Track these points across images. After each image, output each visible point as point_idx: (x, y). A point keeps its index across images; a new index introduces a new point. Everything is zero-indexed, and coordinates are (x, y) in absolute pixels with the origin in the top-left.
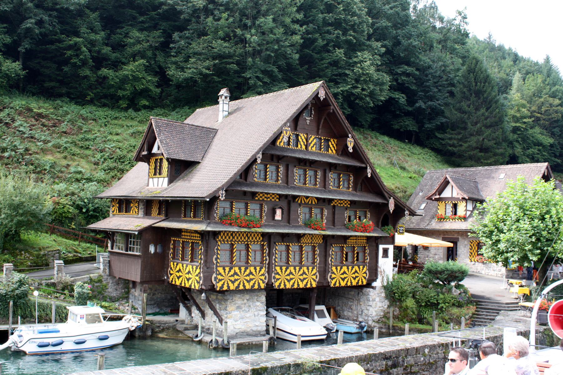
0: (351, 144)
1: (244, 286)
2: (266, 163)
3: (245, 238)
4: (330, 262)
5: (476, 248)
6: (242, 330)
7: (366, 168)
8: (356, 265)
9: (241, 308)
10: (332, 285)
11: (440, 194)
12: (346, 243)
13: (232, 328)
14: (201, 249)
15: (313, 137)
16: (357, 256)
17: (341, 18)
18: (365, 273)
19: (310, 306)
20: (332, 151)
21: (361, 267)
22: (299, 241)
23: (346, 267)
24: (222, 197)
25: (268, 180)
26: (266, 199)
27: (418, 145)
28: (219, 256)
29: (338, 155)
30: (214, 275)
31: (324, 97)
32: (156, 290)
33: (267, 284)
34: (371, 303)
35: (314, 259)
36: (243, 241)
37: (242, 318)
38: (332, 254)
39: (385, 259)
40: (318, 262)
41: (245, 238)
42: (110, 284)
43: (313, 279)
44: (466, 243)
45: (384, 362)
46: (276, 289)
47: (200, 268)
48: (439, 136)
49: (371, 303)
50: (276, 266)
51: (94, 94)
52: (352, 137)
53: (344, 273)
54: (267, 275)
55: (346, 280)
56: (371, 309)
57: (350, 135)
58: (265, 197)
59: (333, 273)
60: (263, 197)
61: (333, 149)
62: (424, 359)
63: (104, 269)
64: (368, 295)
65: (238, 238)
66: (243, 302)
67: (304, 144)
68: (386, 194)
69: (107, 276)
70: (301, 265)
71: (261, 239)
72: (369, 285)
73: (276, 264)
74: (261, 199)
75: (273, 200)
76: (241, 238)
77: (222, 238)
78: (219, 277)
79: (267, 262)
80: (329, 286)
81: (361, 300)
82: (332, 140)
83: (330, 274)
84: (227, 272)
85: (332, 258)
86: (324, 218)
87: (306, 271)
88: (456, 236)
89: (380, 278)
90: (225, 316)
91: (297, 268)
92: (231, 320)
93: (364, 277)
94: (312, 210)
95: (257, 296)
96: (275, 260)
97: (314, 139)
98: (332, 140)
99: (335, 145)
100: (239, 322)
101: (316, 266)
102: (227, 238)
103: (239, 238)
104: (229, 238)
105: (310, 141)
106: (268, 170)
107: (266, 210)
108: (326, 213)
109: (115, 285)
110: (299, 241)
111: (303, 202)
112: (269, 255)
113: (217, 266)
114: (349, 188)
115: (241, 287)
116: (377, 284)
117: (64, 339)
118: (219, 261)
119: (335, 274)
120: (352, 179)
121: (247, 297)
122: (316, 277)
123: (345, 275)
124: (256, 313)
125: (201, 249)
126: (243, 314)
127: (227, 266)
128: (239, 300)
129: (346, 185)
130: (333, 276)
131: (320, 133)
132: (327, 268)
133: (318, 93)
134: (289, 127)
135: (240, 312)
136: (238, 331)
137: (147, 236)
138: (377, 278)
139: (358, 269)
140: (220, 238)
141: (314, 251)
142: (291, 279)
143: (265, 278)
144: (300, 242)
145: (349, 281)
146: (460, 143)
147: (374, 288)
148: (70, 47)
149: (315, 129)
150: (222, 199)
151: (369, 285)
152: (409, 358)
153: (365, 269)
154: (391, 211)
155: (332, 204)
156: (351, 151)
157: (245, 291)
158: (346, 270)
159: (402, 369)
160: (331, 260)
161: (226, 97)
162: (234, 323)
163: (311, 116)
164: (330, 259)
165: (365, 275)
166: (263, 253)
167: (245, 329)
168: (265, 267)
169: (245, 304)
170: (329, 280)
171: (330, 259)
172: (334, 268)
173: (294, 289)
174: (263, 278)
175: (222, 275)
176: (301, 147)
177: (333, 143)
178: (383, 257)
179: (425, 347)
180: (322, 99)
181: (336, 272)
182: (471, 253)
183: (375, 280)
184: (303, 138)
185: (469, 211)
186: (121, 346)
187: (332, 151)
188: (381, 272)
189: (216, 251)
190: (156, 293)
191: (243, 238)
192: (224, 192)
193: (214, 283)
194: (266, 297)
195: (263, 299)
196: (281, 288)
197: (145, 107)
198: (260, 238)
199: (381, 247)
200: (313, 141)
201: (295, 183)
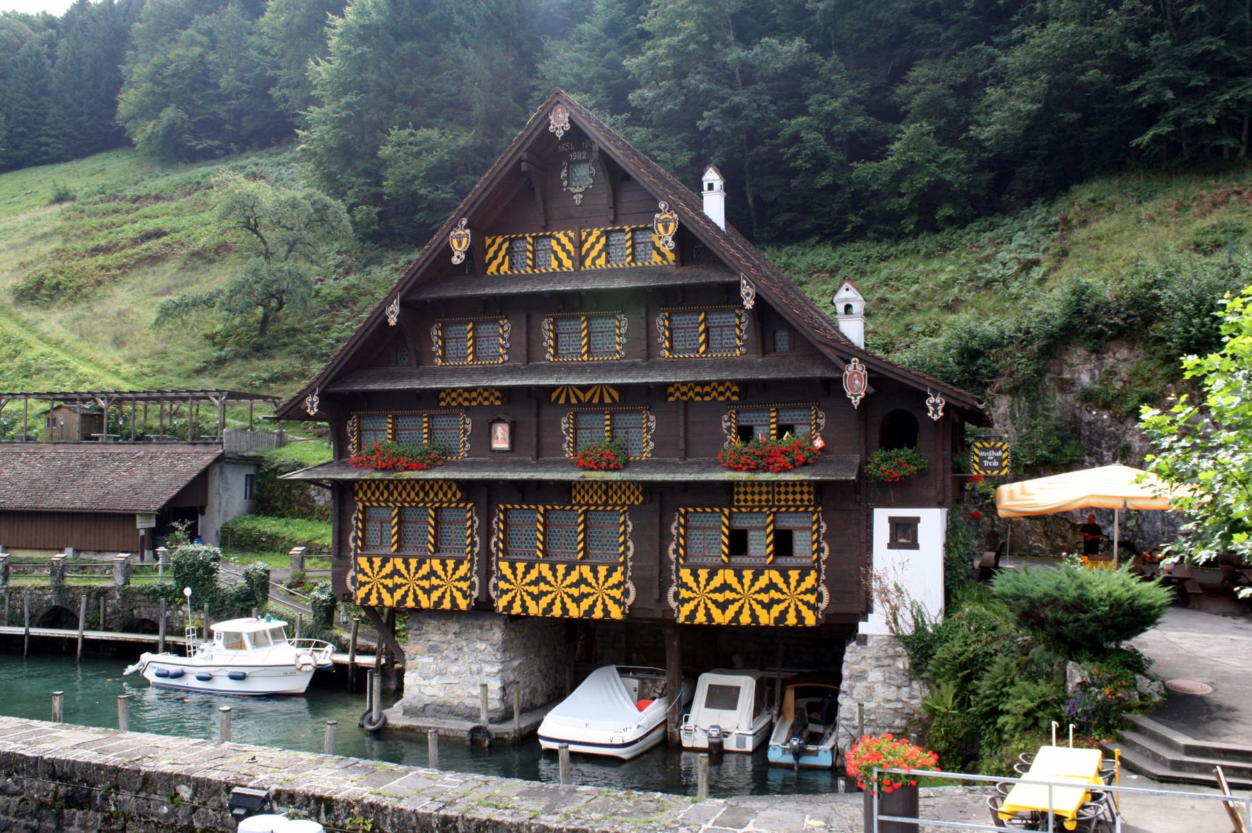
1: (416, 599)
3: (417, 494)
6: (440, 701)
9: (440, 652)
10: (681, 619)
13: (415, 691)
15: (596, 233)
26: (466, 404)
30: (352, 573)
36: (413, 500)
38: (499, 529)
41: (417, 494)
45: (53, 785)
50: (498, 559)
51: (863, 216)
54: (475, 579)
58: (466, 399)
62: (172, 813)
65: (400, 494)
66: (443, 638)
67: (569, 257)
71: (459, 495)
74: (454, 404)
75: (486, 403)
76: (409, 495)
77: (365, 493)
78: (361, 577)
84: (560, 577)
85: (678, 545)
92: (415, 675)
95: (420, 622)
100: (433, 682)
102: (377, 494)
103: (404, 495)
104: (382, 494)
111: (574, 401)
113: (356, 555)
115: (410, 603)
116: (874, 626)
117: (186, 669)
121: (455, 627)
124: (475, 667)
126: (442, 665)
128: (435, 634)
134: (466, 227)
135: (435, 659)
136: (428, 700)
138: (869, 609)
140: (361, 494)
142: (543, 594)
143: (472, 587)
147: (863, 640)
150: (312, 413)
152: (126, 796)
159: (99, 816)
160: (496, 544)
162: (421, 682)
167: (446, 699)
168: (471, 561)
169: (449, 643)
175: (366, 574)
176: (561, 265)
178: (891, 546)
179: (187, 780)
184: (564, 240)
186: (304, 701)
188: (885, 592)
191: (413, 495)
192: (315, 399)
193: (352, 588)
196: (696, 622)
197: (950, 220)
198: (454, 495)
199: (882, 518)
201: (547, 356)
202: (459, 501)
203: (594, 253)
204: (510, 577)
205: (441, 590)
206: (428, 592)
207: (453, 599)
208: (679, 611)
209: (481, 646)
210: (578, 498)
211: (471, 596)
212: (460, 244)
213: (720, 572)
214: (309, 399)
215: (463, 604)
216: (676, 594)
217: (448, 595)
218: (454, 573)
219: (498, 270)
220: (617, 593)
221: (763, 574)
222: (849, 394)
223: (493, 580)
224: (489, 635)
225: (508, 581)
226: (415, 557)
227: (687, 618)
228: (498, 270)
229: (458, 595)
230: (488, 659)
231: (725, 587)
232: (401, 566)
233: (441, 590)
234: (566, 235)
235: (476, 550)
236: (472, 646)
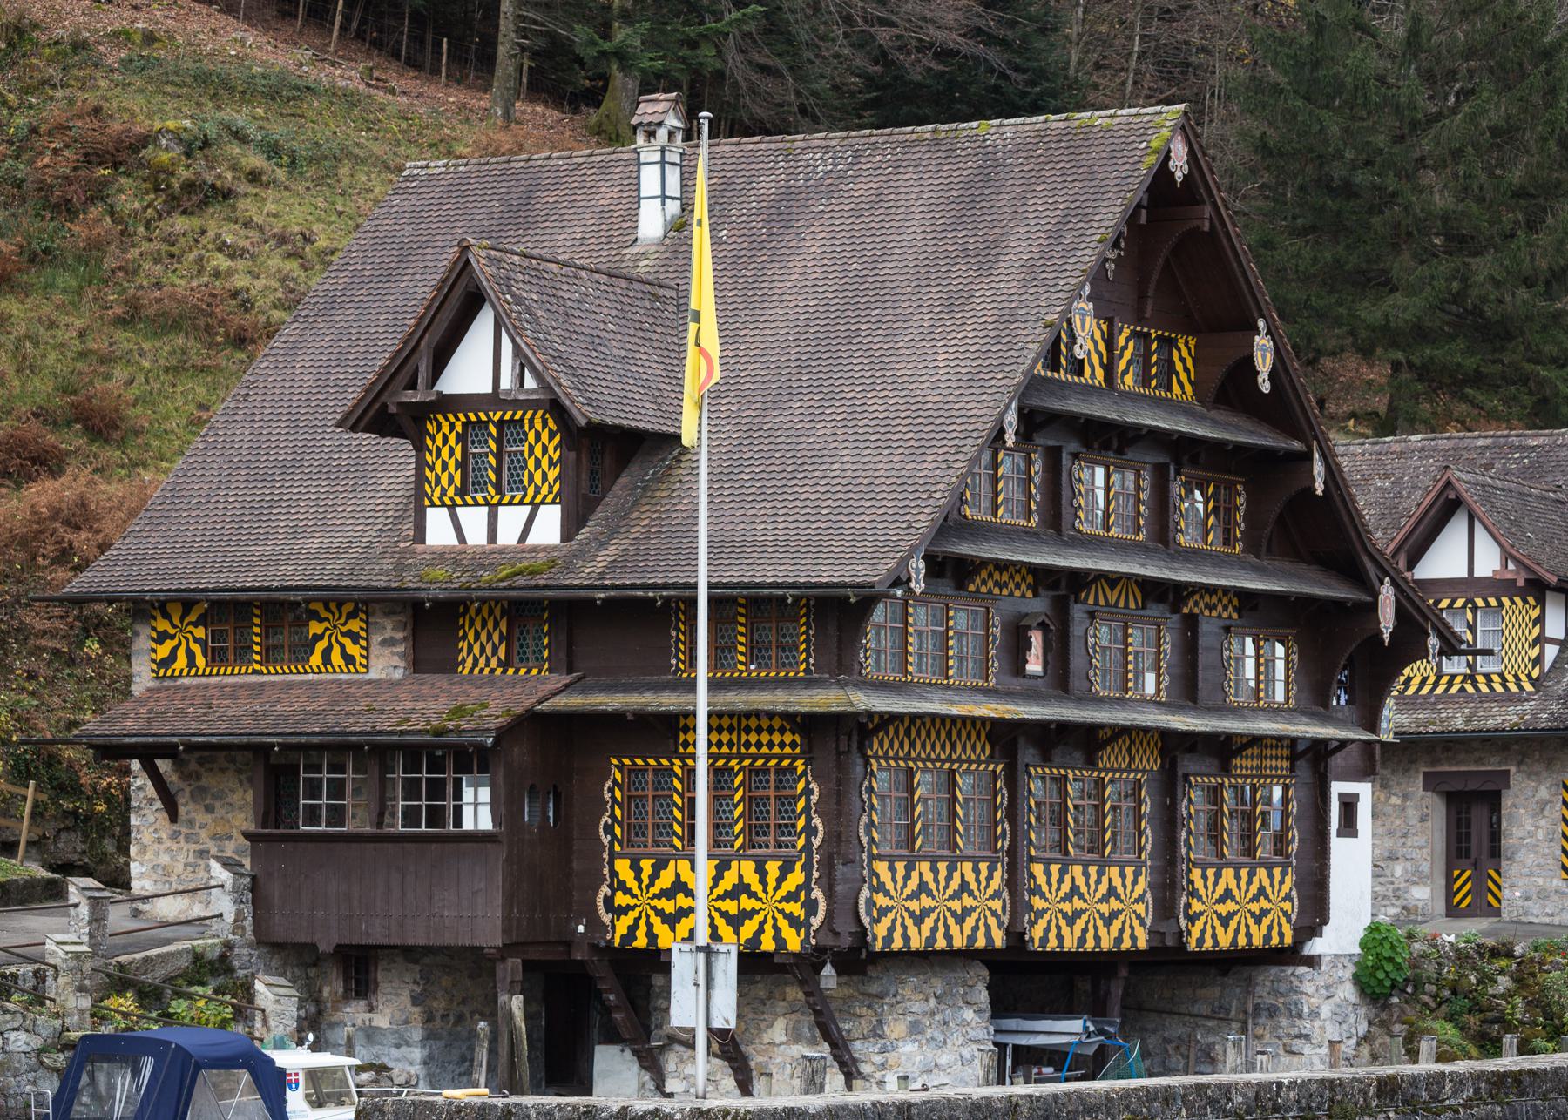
0: (1264, 357)
7: (1308, 457)
9: (922, 1032)
10: (1192, 945)
14: (809, 788)
29: (1202, 402)
34: (1306, 1025)
36: (938, 759)
44: (1543, 792)
47: (807, 868)
52: (1269, 332)
57: (1261, 324)
60: (990, 583)
63: (239, 917)
67: (1178, 374)
69: (251, 946)
73: (875, 851)
80: (1182, 946)
90: (878, 1059)
98: (1181, 343)
125: (807, 792)
126: (929, 1052)
147: (1313, 962)
151: (1291, 955)
155: (1186, 610)
156: (1266, 387)
160: (609, 829)
169: (933, 1014)
172: (623, 866)
173: (1085, 953)
176: (1093, 375)
178: (1339, 835)
185: (1553, 641)
208: (1189, 933)
216: (609, 901)
220: (795, 908)
221: (729, 868)
235: (816, 842)
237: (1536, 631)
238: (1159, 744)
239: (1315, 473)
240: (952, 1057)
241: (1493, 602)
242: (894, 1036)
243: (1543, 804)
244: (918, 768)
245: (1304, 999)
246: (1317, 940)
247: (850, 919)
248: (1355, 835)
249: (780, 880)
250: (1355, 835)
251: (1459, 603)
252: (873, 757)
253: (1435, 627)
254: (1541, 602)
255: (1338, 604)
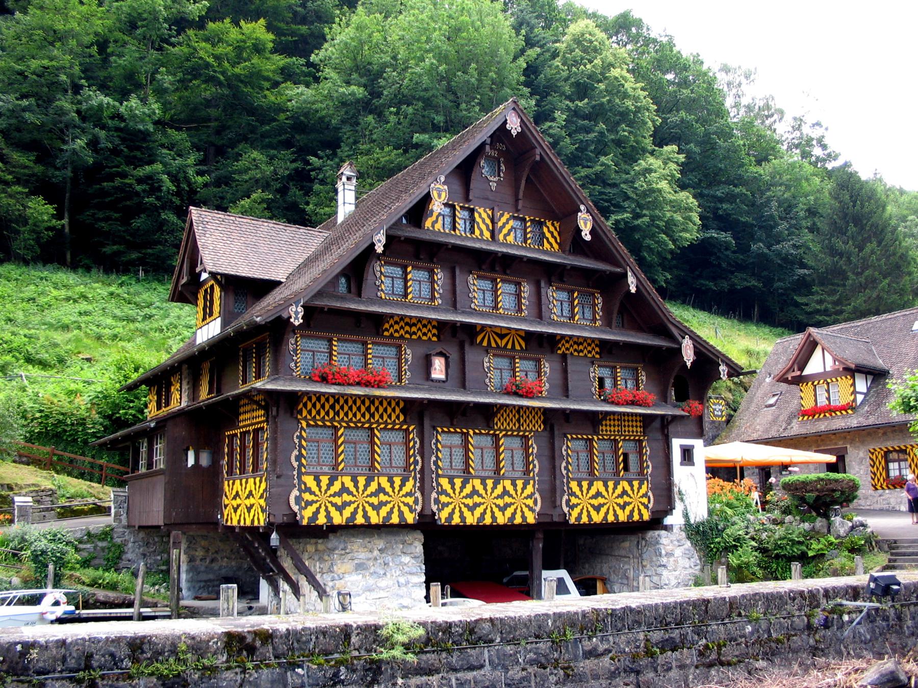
0: (586, 225)
1: (365, 516)
2: (405, 262)
3: (363, 415)
4: (564, 472)
5: (883, 463)
8: (623, 479)
9: (367, 569)
10: (572, 521)
11: (802, 369)
12: (597, 434)
15: (506, 216)
16: (626, 461)
17: (602, 104)
18: (645, 495)
19: (532, 572)
20: (551, 244)
21: (636, 483)
22: (489, 424)
23: (600, 483)
24: (297, 318)
25: (410, 297)
27: (765, 323)
28: (304, 452)
29: (564, 252)
30: (295, 493)
31: (519, 130)
32: (216, 552)
33: (421, 515)
34: (664, 560)
35: (528, 463)
36: (359, 421)
37: (370, 590)
39: (688, 469)
40: (536, 470)
41: (363, 415)
42: (130, 545)
43: (527, 506)
44: (861, 454)
46: (443, 526)
48: (800, 300)
49: (664, 560)
50: (438, 476)
53: (598, 494)
54: (418, 494)
55: (603, 510)
56: (665, 573)
57: (582, 207)
59: (573, 494)
61: (552, 240)
64: (658, 543)
65: (346, 414)
66: (370, 555)
68: (675, 332)
69: (124, 527)
70: (498, 477)
71: (402, 418)
72: (656, 523)
73: (440, 472)
74: (396, 335)
75: (425, 338)
76: (355, 415)
77: (310, 412)
79: (418, 468)
80: (566, 522)
81: (644, 556)
82: (549, 224)
83: (565, 497)
85: (568, 463)
86: (544, 379)
87: (510, 488)
88: (840, 445)
89: (679, 507)
90: (331, 584)
91: (490, 483)
93: (643, 504)
94: (515, 363)
95: (404, 543)
96: (436, 463)
97: (508, 220)
99: (556, 234)
101: (533, 478)
102: (323, 413)
103: (350, 415)
104: (327, 413)
105: (500, 224)
106: (409, 277)
107: (410, 358)
108: (548, 370)
109: (140, 546)
110: (489, 424)
111: (494, 345)
112: (422, 452)
113: (300, 474)
114: (594, 320)
116: (675, 519)
118: (304, 461)
119: (577, 497)
120: (599, 301)
121: (380, 543)
122: (535, 502)
123: (601, 500)
126: (371, 581)
127: (325, 474)
128: (360, 549)
129: (588, 315)
130: (574, 500)
131: (519, 207)
132: (558, 482)
133: (505, 122)
134: (444, 183)
135: (364, 576)
137: (179, 431)
139: (628, 488)
140: (305, 413)
141: (526, 448)
143: (416, 502)
144: (492, 428)
145: (611, 512)
146: (838, 308)
147: (667, 528)
148: (140, 181)
149: (511, 200)
150: (297, 323)
153: (644, 488)
154: (689, 364)
156: (588, 238)
157: (369, 529)
158: (602, 489)
161: (349, 179)
163: (499, 175)
164: (564, 464)
165: (645, 500)
166: (408, 449)
168: (415, 478)
169: (376, 559)
170: (566, 509)
171: (564, 464)
172: (574, 485)
173: (485, 526)
174: (410, 500)
175: (312, 493)
176: (482, 233)
177: (552, 229)
178: (682, 464)
180: (514, 133)
181: (578, 493)
182: (875, 474)
183: (669, 511)
184: (484, 215)
187: (551, 244)
189: (296, 441)
190: (219, 557)
192: (300, 309)
193: (296, 508)
194: (424, 545)
195: (419, 549)
196: (453, 523)
198: (398, 417)
199: (677, 444)
200: (507, 222)
201: (473, 306)
202: (402, 424)
203: (505, 231)
204: (450, 491)
205: (389, 506)
206: (340, 509)
207: (401, 513)
208: (570, 514)
209: (406, 559)
210: (499, 424)
211: (416, 510)
212: (439, 196)
213: (595, 483)
214: (293, 308)
215: (410, 518)
217: (396, 510)
218: (401, 489)
219: (433, 226)
222: (685, 359)
223: (434, 495)
224: (411, 549)
225: (448, 495)
226: (363, 475)
227: (576, 519)
228: (433, 226)
229: (405, 510)
230: (415, 570)
231: (598, 494)
232: (349, 484)
233: (389, 506)
234: (485, 211)
236: (397, 560)
237: (852, 389)
238: (542, 418)
239: (629, 282)
240: (391, 583)
241: (834, 380)
242: (340, 572)
243: (862, 460)
244: (341, 426)
245: (662, 547)
246: (669, 517)
247: (286, 507)
248: (693, 464)
249: (401, 487)
250: (693, 464)
251: (821, 382)
252: (303, 419)
253: (722, 361)
254: (853, 377)
255: (659, 348)
